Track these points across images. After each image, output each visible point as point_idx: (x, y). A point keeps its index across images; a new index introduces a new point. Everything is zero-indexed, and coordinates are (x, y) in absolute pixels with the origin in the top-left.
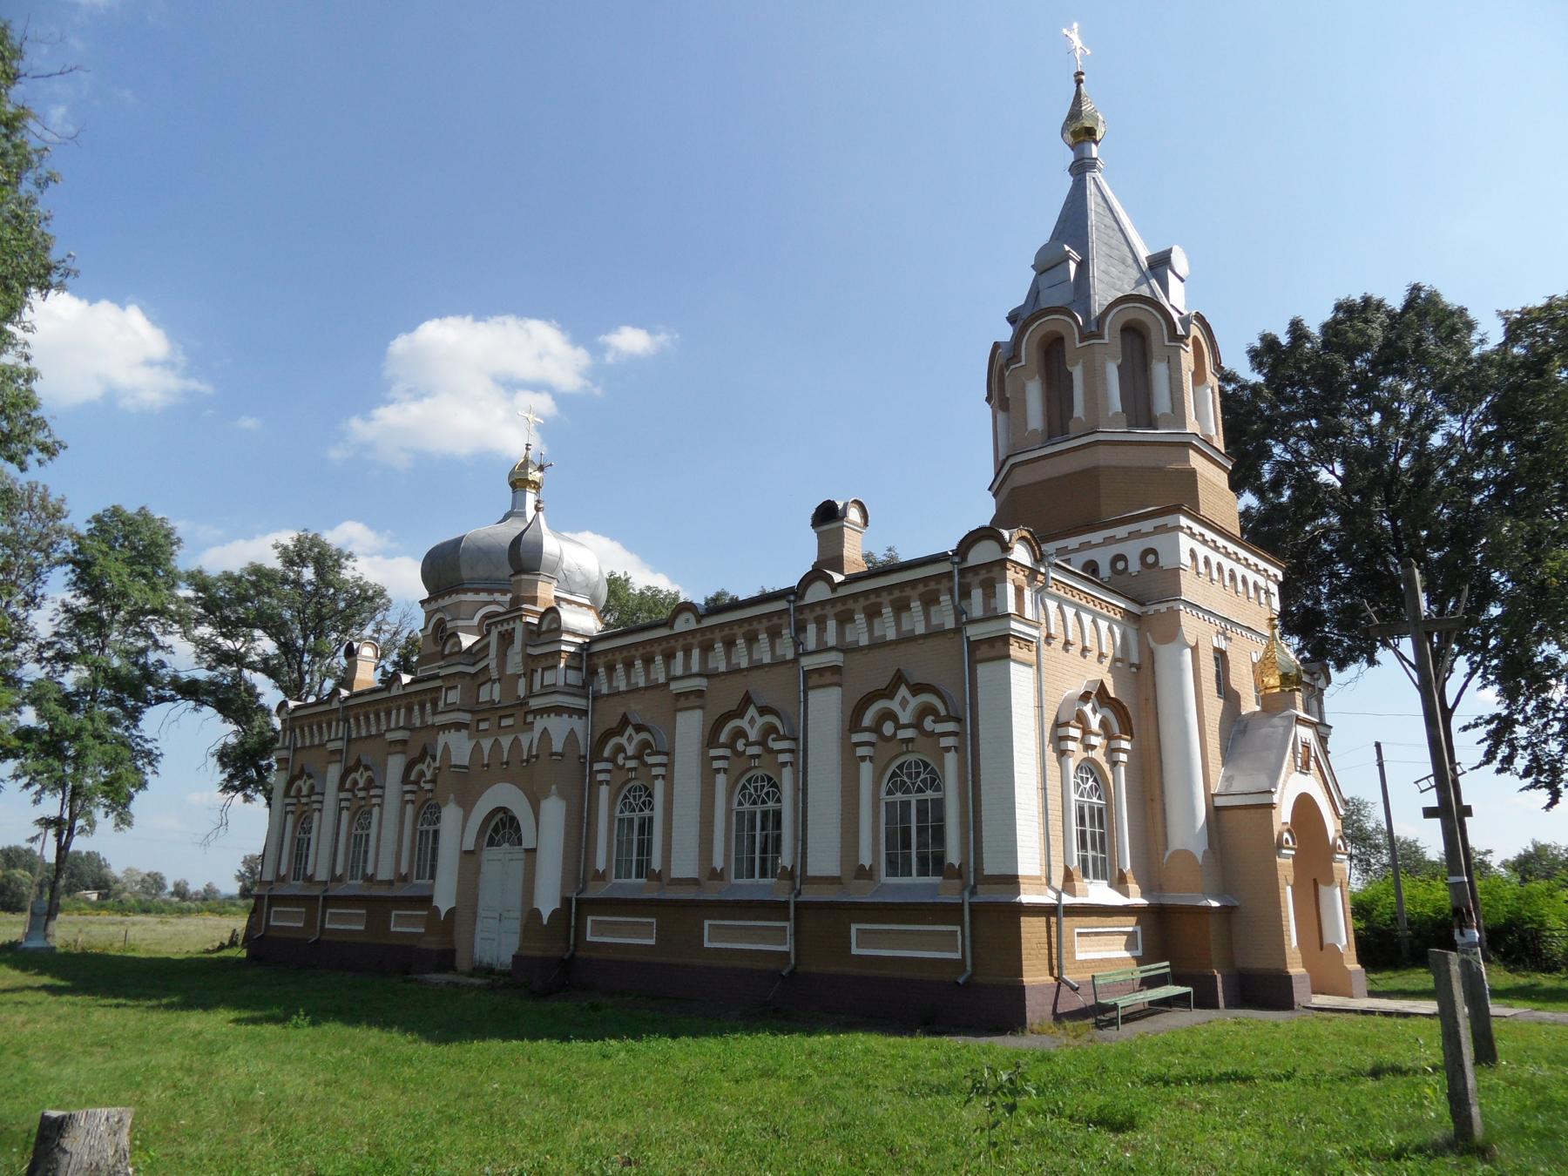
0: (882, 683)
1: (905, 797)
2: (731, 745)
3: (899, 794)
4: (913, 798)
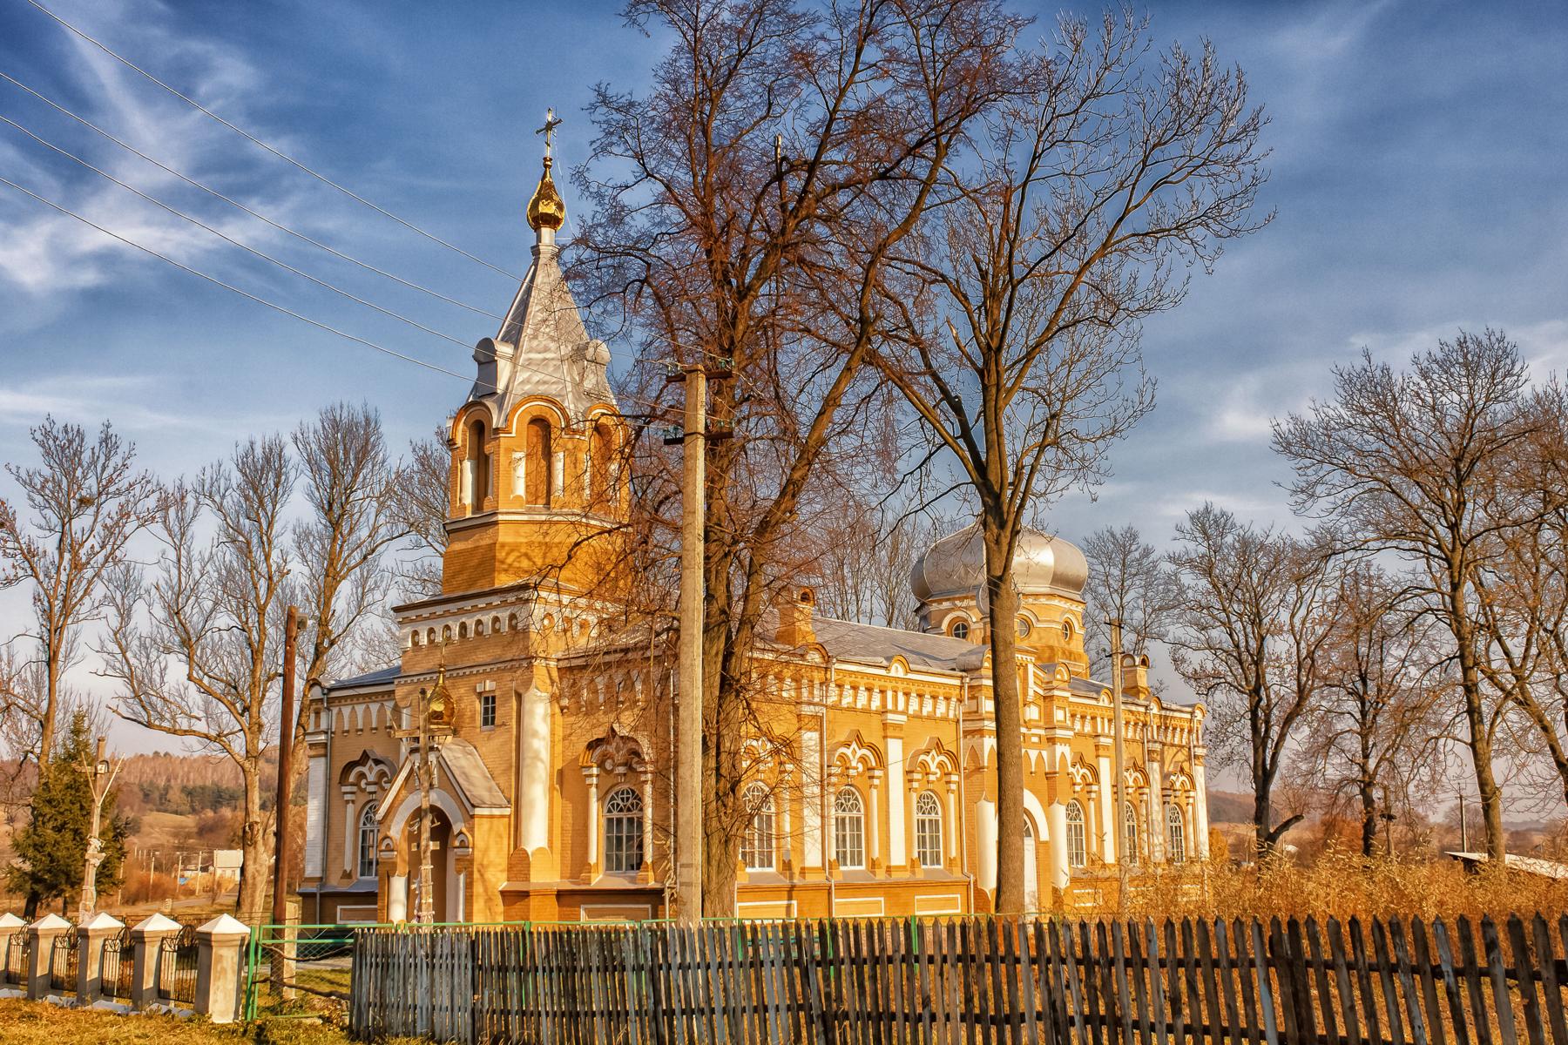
1: (621, 815)
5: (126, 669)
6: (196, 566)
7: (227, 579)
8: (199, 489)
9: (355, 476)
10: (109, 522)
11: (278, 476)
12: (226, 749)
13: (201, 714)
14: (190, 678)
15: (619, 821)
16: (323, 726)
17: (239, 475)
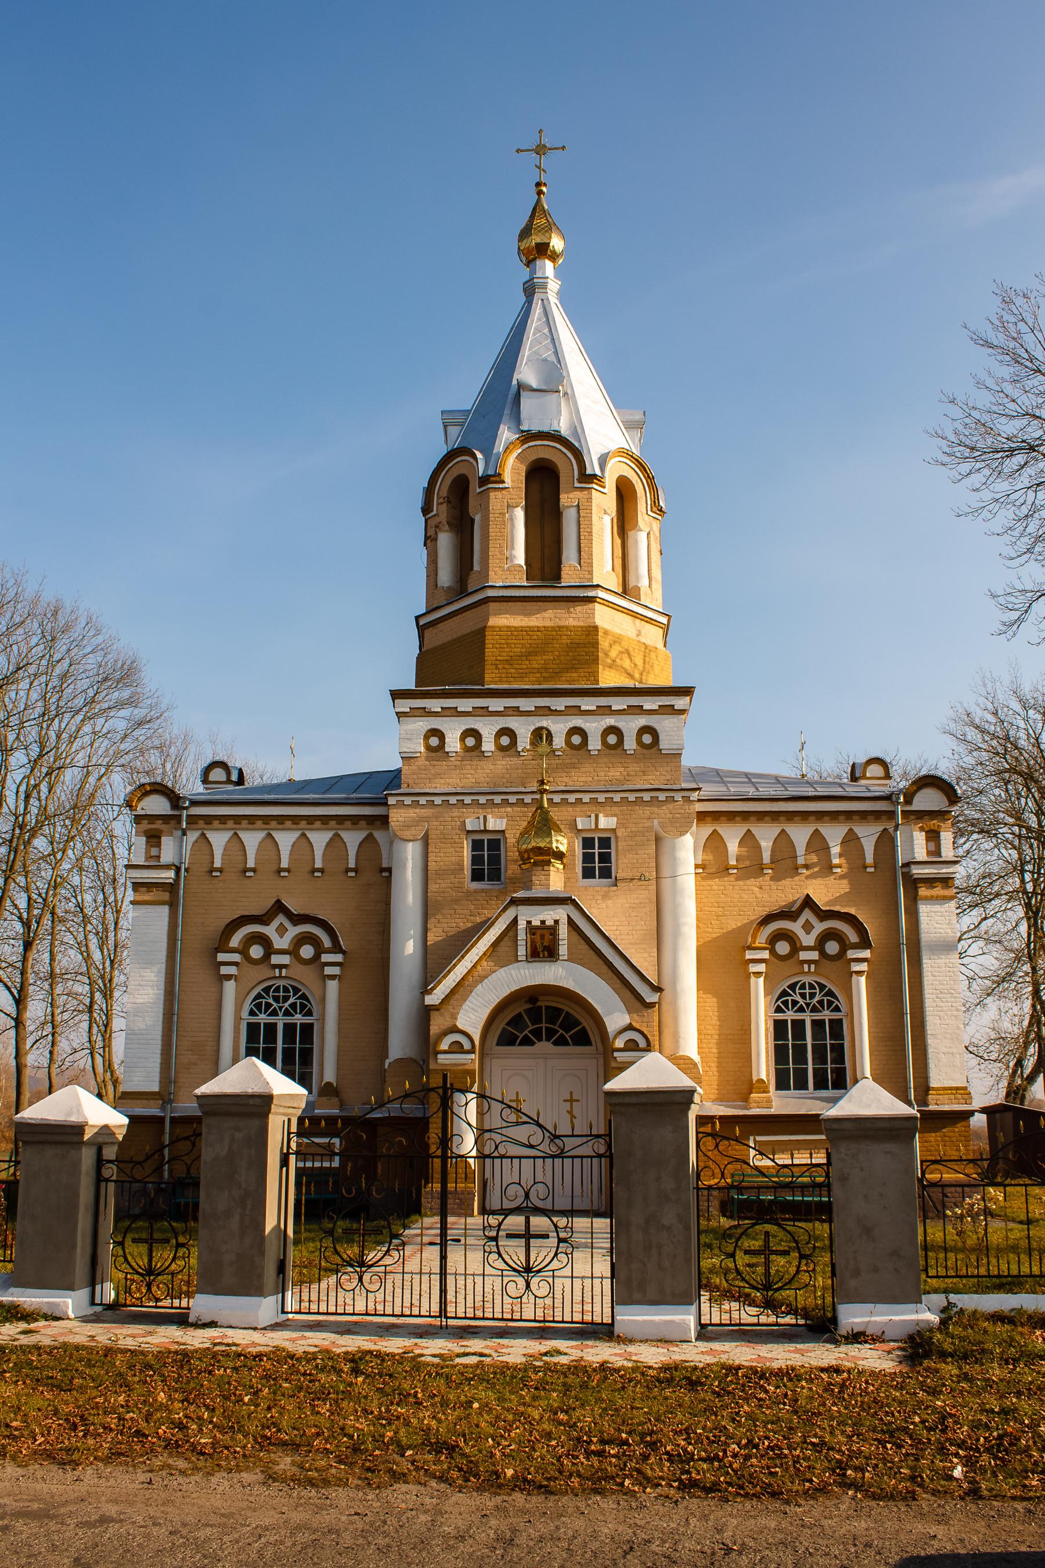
0: (258, 908)
2: (244, 951)
3: (298, 1016)
4: (280, 1021)
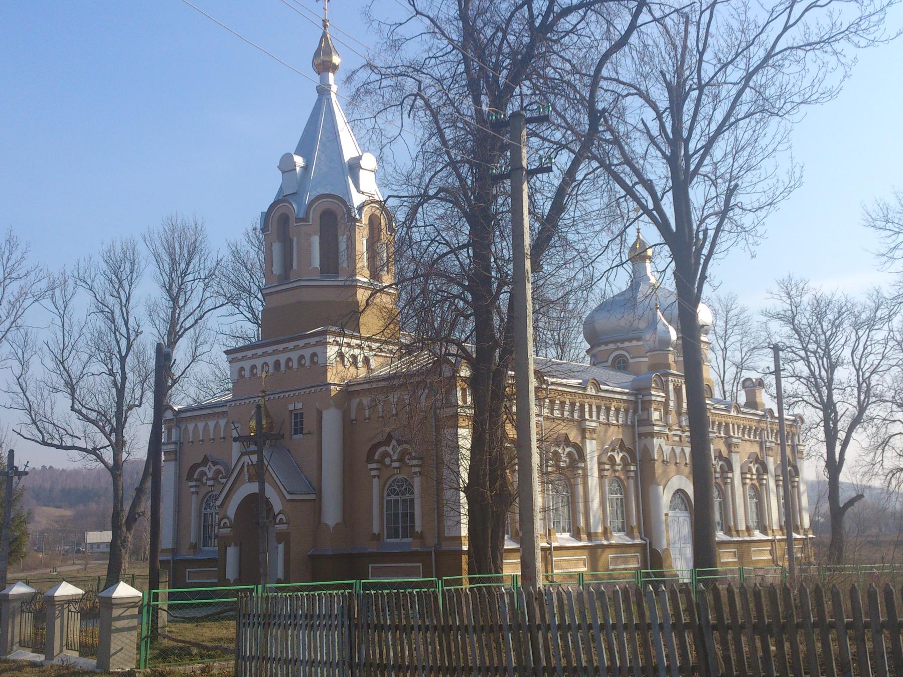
1: (397, 497)
5: (26, 403)
6: (76, 329)
7: (98, 343)
8: (76, 275)
9: (188, 264)
10: (13, 300)
11: (133, 264)
12: (100, 458)
13: (80, 435)
14: (73, 409)
15: (397, 501)
16: (173, 439)
17: (105, 265)
